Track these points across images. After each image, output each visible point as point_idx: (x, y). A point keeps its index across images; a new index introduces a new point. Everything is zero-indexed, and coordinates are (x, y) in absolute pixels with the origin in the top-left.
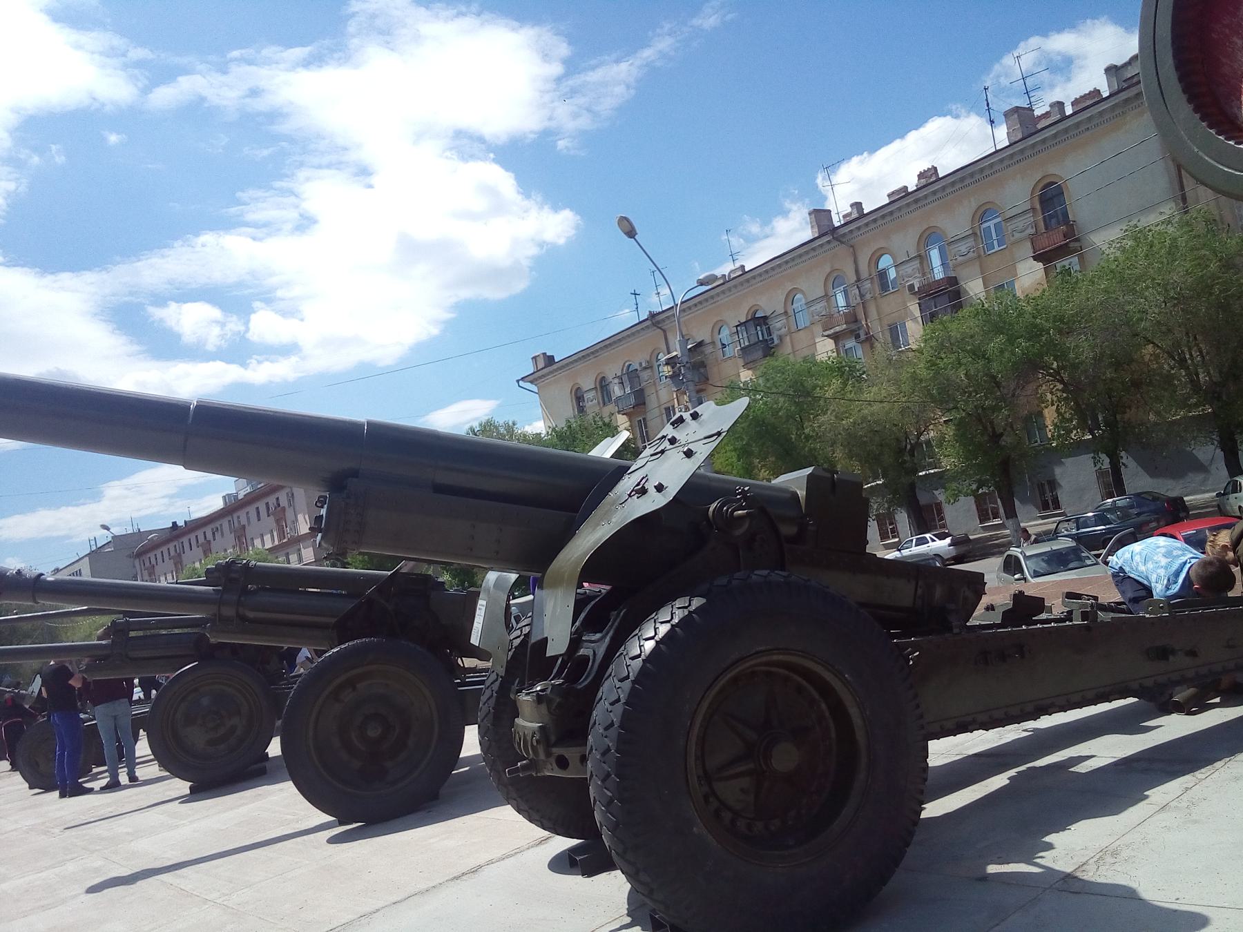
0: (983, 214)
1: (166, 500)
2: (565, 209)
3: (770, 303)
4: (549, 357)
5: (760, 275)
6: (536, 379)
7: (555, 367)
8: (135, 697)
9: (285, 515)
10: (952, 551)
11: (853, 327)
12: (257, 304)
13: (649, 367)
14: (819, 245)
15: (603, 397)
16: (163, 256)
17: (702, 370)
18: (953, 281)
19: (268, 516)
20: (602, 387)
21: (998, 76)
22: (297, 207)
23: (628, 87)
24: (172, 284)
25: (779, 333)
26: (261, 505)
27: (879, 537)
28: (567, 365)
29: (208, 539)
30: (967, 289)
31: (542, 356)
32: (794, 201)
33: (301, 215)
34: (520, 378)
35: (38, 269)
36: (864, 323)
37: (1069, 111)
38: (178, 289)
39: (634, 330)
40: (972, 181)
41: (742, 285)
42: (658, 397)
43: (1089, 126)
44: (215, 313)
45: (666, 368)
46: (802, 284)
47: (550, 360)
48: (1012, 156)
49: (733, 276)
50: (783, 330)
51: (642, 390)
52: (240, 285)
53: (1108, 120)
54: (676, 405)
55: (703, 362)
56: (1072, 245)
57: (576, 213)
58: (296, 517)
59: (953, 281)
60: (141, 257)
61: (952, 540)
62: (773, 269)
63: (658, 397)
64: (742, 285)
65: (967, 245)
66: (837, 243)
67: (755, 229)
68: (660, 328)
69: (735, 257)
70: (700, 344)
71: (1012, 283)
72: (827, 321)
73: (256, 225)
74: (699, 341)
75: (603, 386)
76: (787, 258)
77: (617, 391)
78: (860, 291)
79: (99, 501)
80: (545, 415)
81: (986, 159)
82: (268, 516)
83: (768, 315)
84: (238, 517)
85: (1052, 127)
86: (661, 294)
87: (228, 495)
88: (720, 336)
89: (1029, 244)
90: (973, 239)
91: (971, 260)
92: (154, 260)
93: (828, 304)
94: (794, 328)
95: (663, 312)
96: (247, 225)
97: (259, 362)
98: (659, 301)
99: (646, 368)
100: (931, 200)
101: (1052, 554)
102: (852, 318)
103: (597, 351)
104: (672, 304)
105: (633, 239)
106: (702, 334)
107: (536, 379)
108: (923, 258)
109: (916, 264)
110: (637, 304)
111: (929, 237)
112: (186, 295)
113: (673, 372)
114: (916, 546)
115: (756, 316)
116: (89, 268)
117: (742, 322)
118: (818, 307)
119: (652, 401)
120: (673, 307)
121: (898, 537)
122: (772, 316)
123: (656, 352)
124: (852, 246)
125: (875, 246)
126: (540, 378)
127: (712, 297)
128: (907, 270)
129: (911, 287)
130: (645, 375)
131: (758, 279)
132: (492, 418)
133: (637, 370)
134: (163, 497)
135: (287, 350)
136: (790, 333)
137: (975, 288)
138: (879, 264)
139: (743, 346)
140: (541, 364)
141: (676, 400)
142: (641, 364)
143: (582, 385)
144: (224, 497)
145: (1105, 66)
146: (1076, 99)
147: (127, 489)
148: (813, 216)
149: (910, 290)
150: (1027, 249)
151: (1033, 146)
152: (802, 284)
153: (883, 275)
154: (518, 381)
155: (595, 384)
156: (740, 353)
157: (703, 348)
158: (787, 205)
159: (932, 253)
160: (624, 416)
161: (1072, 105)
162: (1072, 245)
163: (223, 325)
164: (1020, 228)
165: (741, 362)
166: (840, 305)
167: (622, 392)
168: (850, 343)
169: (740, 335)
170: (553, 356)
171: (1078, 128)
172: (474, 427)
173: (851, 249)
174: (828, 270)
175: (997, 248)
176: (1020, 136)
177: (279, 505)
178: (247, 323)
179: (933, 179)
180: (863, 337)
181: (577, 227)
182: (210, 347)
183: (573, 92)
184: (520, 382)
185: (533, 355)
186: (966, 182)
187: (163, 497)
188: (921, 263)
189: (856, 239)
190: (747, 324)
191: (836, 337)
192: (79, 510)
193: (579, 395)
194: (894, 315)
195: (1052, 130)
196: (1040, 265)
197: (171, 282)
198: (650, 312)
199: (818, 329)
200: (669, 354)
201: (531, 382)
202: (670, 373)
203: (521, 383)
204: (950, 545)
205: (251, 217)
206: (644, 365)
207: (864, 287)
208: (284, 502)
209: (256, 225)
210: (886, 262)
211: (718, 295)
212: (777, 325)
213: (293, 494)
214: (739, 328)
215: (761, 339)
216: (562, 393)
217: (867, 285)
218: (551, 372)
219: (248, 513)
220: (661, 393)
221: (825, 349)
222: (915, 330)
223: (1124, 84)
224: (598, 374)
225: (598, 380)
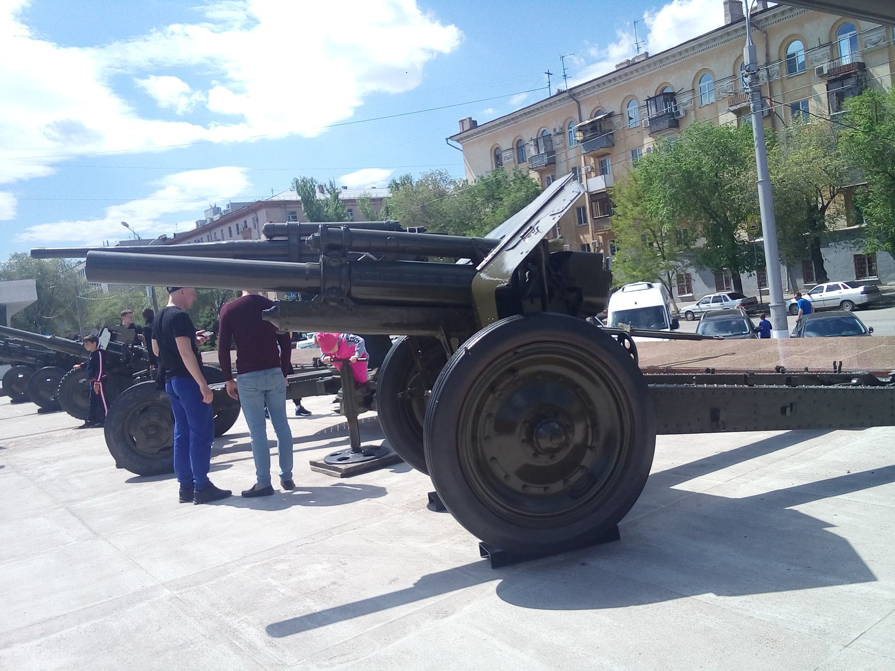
1: (150, 223)
2: (451, 24)
3: (678, 81)
4: (473, 121)
5: (673, 56)
6: (462, 139)
8: (753, 320)
9: (251, 234)
10: (865, 299)
12: (214, 82)
13: (562, 133)
14: (733, 31)
15: (518, 156)
16: (145, 40)
18: (862, 66)
19: (238, 234)
20: (518, 148)
22: (244, 10)
24: (152, 63)
25: (684, 107)
26: (233, 225)
27: (757, 285)
28: (490, 128)
31: (468, 120)
32: (624, 31)
33: (248, 17)
34: (448, 137)
35: (55, 44)
38: (157, 67)
41: (626, 75)
44: (185, 87)
45: (578, 134)
46: (713, 66)
47: (474, 124)
49: (637, 61)
50: (689, 105)
51: (553, 152)
52: (201, 67)
53: (791, 16)
57: (460, 28)
60: (129, 40)
61: (865, 288)
62: (686, 51)
64: (626, 75)
65: (879, 35)
67: (593, 52)
68: (576, 100)
70: (610, 115)
73: (213, 21)
74: (610, 112)
75: (519, 147)
77: (532, 151)
79: (104, 219)
80: (467, 168)
82: (238, 234)
83: (676, 92)
84: (215, 233)
86: (568, 76)
87: (200, 221)
90: (829, 48)
91: (883, 48)
92: (138, 43)
96: (207, 20)
97: (216, 126)
99: (558, 134)
100: (779, 18)
101: (720, 323)
103: (517, 117)
106: (612, 106)
107: (462, 139)
110: (549, 82)
112: (160, 70)
114: (827, 291)
116: (91, 45)
117: (651, 97)
118: (726, 84)
119: (561, 157)
121: (692, 293)
122: (680, 93)
124: (765, 32)
125: (787, 33)
126: (466, 137)
127: (626, 75)
128: (817, 55)
129: (820, 70)
130: (557, 139)
132: (410, 174)
134: (149, 220)
135: (238, 119)
138: (788, 51)
142: (555, 130)
144: (197, 222)
147: (123, 212)
148: (728, 5)
150: (647, 132)
152: (713, 66)
154: (447, 139)
157: (612, 119)
158: (619, 33)
160: (536, 173)
163: (189, 95)
167: (536, 153)
170: (476, 121)
172: (396, 179)
177: (246, 227)
178: (207, 96)
181: (461, 39)
182: (179, 112)
184: (449, 140)
185: (461, 119)
187: (149, 220)
188: (831, 49)
189: (770, 26)
192: (89, 224)
193: (497, 153)
197: (151, 60)
198: (559, 90)
199: (725, 105)
200: (580, 122)
201: (458, 141)
203: (449, 141)
204: (862, 293)
205: (209, 15)
206: (558, 131)
207: (772, 69)
208: (250, 224)
209: (213, 21)
210: (796, 47)
211: (631, 73)
212: (683, 100)
213: (257, 219)
217: (776, 67)
219: (222, 231)
225: (493, 150)
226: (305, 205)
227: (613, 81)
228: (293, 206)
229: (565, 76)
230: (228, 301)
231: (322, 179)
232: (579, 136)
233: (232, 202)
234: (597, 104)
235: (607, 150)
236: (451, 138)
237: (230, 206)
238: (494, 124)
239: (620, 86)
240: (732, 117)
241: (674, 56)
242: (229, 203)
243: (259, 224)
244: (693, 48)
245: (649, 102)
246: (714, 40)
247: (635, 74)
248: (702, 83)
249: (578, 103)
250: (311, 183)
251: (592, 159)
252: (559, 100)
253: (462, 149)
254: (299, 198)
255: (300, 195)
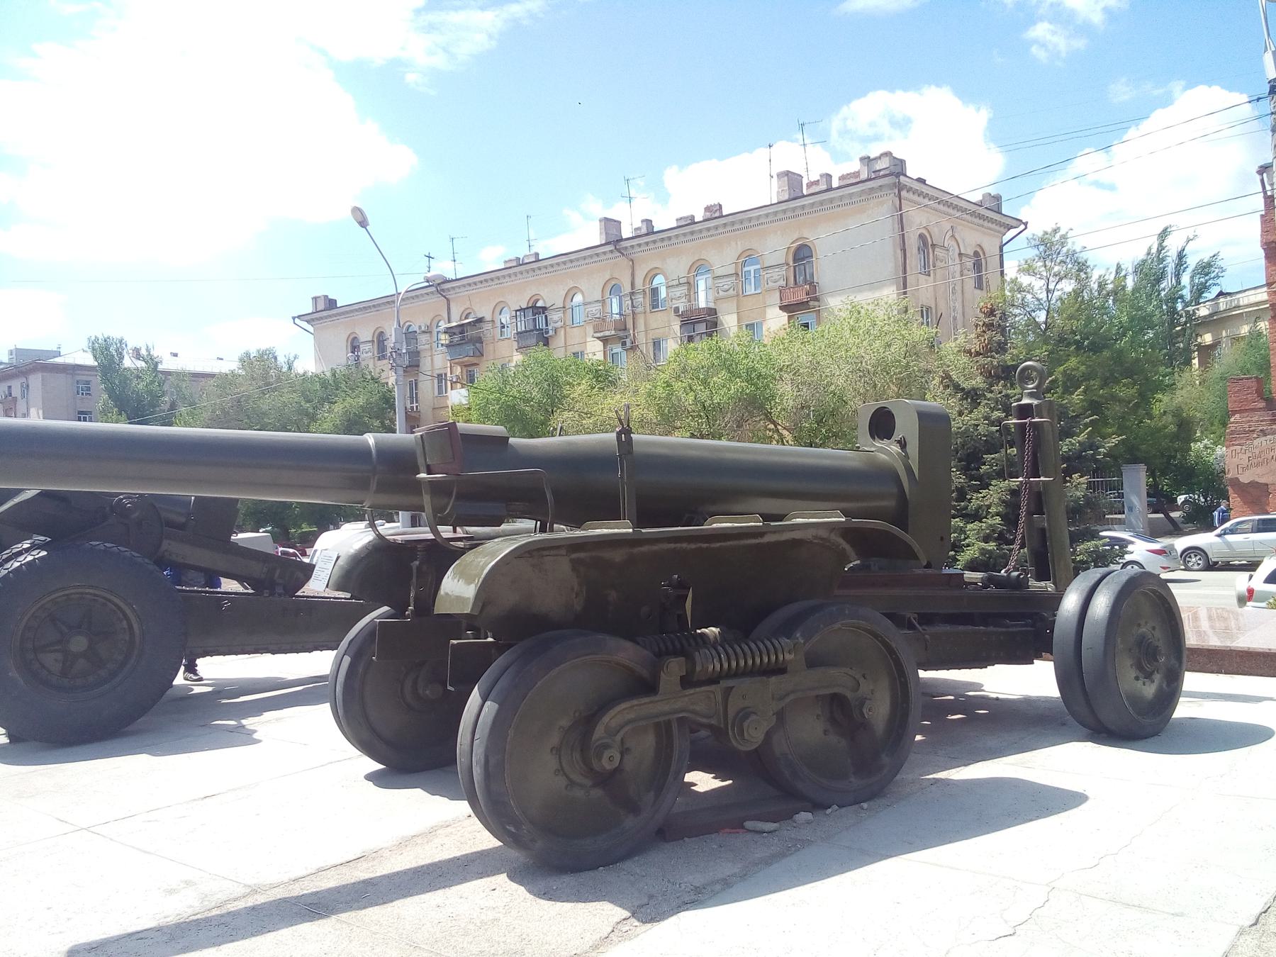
0: (748, 257)
3: (550, 295)
6: (313, 320)
7: (334, 312)
11: (621, 334)
17: (478, 345)
18: (712, 312)
20: (379, 342)
21: (846, 119)
23: (490, 37)
25: (556, 325)
28: (347, 312)
29: (13, 395)
30: (724, 322)
36: (631, 332)
37: (835, 184)
39: (498, 274)
40: (724, 230)
42: (432, 360)
43: (840, 203)
45: (443, 336)
47: (331, 304)
48: (776, 213)
49: (526, 261)
54: (449, 375)
55: (481, 338)
56: (811, 303)
58: (28, 410)
59: (712, 312)
62: (558, 264)
63: (432, 360)
64: (540, 269)
66: (619, 254)
69: (532, 243)
70: (480, 320)
71: (761, 324)
72: (599, 323)
76: (573, 257)
78: (632, 303)
81: (757, 210)
83: (547, 306)
85: (564, 257)
88: (501, 316)
89: (777, 294)
90: (686, 288)
93: (564, 315)
94: (569, 322)
95: (457, 280)
98: (444, 268)
99: (424, 332)
102: (622, 327)
103: (379, 305)
104: (395, 292)
105: (364, 229)
106: (484, 311)
108: (691, 286)
109: (683, 290)
111: (699, 267)
113: (451, 342)
115: (537, 305)
119: (426, 364)
120: (394, 295)
123: (437, 319)
124: (632, 261)
126: (318, 319)
127: (498, 278)
129: (676, 310)
130: (423, 338)
131: (544, 271)
133: (416, 332)
136: (564, 326)
137: (729, 321)
139: (519, 330)
140: (321, 306)
141: (449, 369)
142: (420, 327)
143: (360, 336)
145: (860, 156)
146: (843, 175)
148: (603, 223)
149: (675, 312)
150: (775, 298)
151: (794, 209)
153: (655, 291)
154: (294, 318)
155: (373, 337)
156: (516, 336)
159: (699, 282)
161: (840, 179)
162: (811, 303)
164: (774, 278)
165: (515, 345)
166: (613, 312)
168: (617, 349)
169: (519, 319)
171: (812, 208)
173: (631, 263)
174: (608, 277)
175: (660, 309)
176: (786, 197)
177: (10, 395)
179: (717, 214)
180: (629, 344)
183: (431, 28)
186: (736, 227)
188: (689, 290)
190: (526, 311)
191: (605, 341)
193: (355, 344)
194: (657, 331)
195: (810, 199)
196: (785, 315)
199: (590, 330)
200: (449, 322)
201: (308, 322)
202: (447, 342)
203: (297, 320)
206: (423, 328)
207: (637, 300)
208: (16, 392)
212: (554, 316)
214: (518, 313)
215: (538, 327)
216: (338, 338)
218: (330, 316)
220: (436, 358)
221: (594, 351)
222: (671, 346)
223: (873, 174)
224: (377, 328)
226: (104, 374)
227: (490, 281)
228: (87, 373)
229: (454, 261)
230: (1087, 551)
231: (134, 340)
232: (444, 339)
233: (17, 347)
234: (467, 305)
235: (474, 360)
236: (299, 317)
237: (14, 353)
238: (351, 308)
239: (491, 290)
240: (599, 345)
241: (655, 243)
242: (13, 348)
243: (30, 393)
244: (564, 263)
245: (518, 313)
246: (585, 258)
247: (507, 279)
248: (748, 266)
249: (448, 300)
250: (119, 345)
251: (459, 368)
252: (647, 243)
253: (313, 332)
254: (96, 364)
255: (96, 360)
